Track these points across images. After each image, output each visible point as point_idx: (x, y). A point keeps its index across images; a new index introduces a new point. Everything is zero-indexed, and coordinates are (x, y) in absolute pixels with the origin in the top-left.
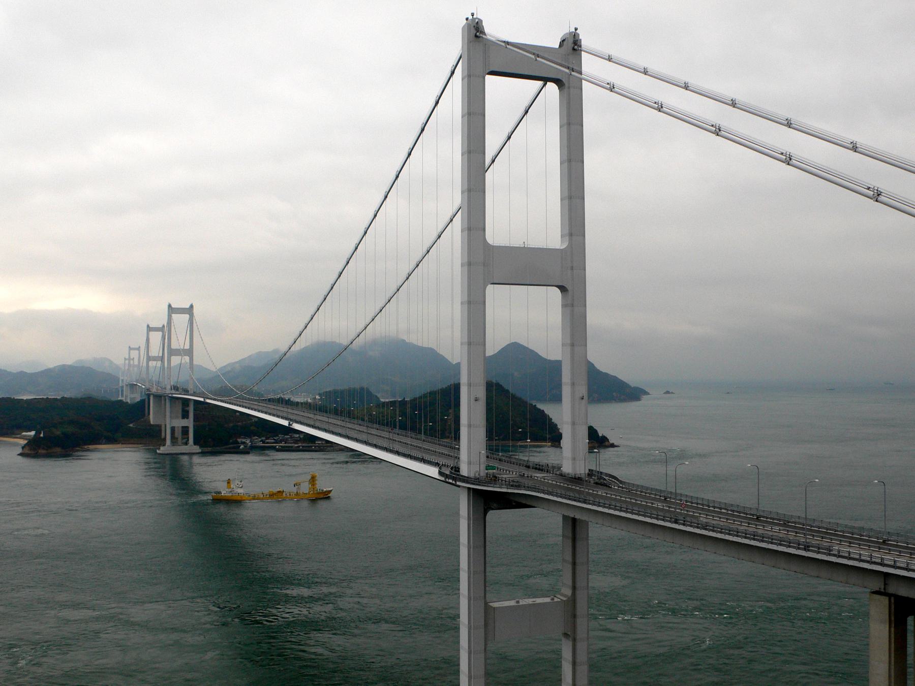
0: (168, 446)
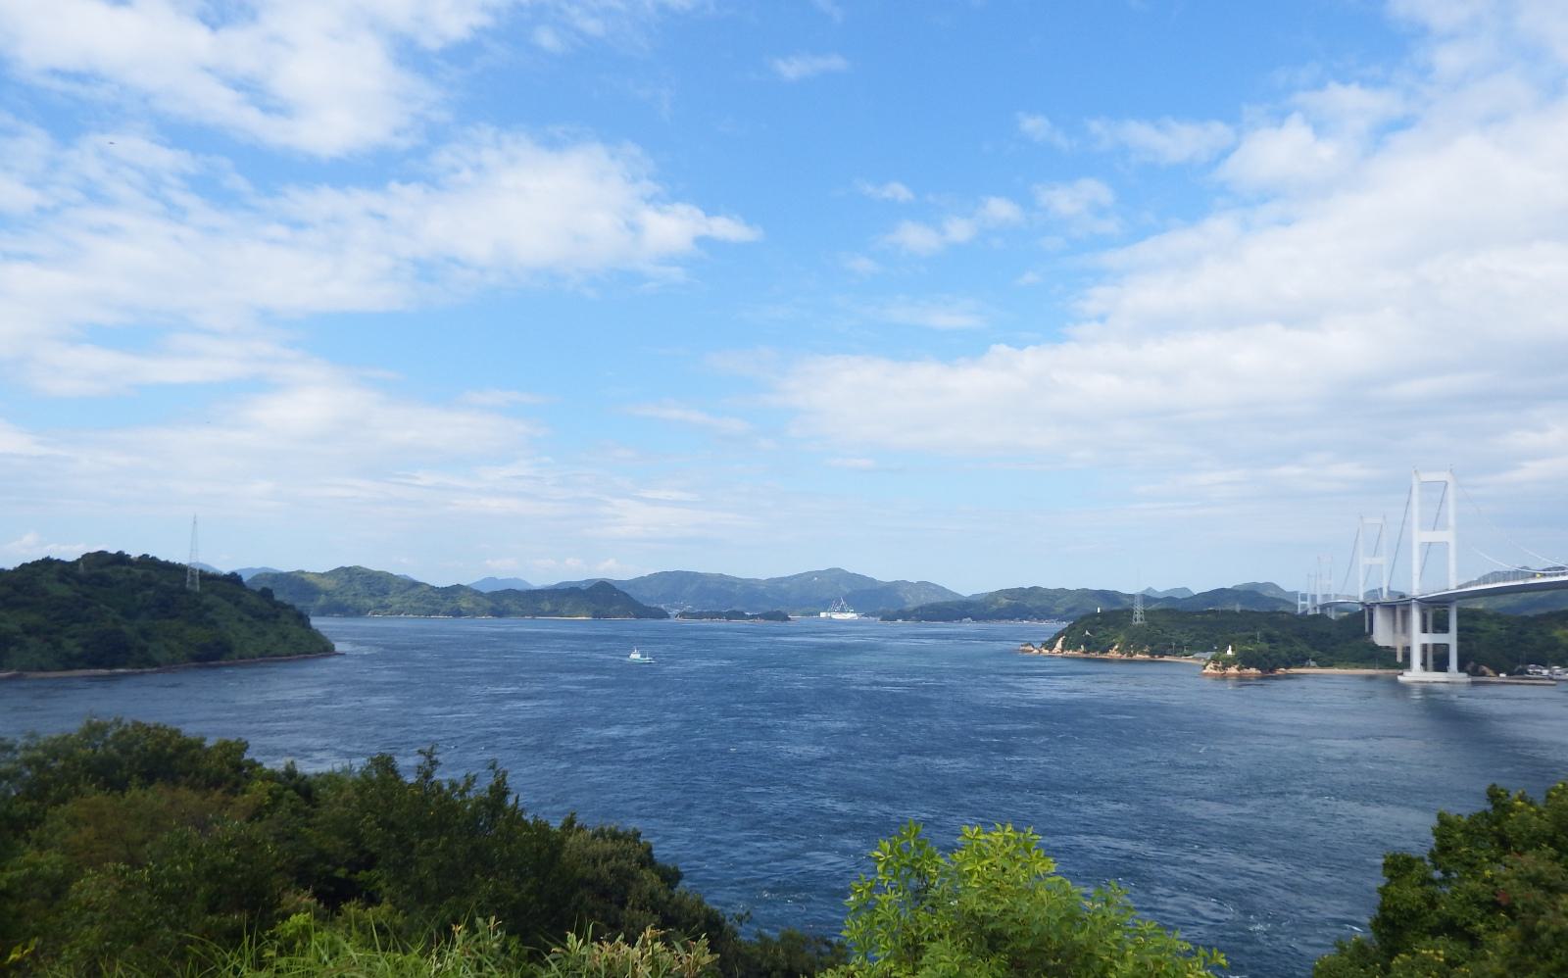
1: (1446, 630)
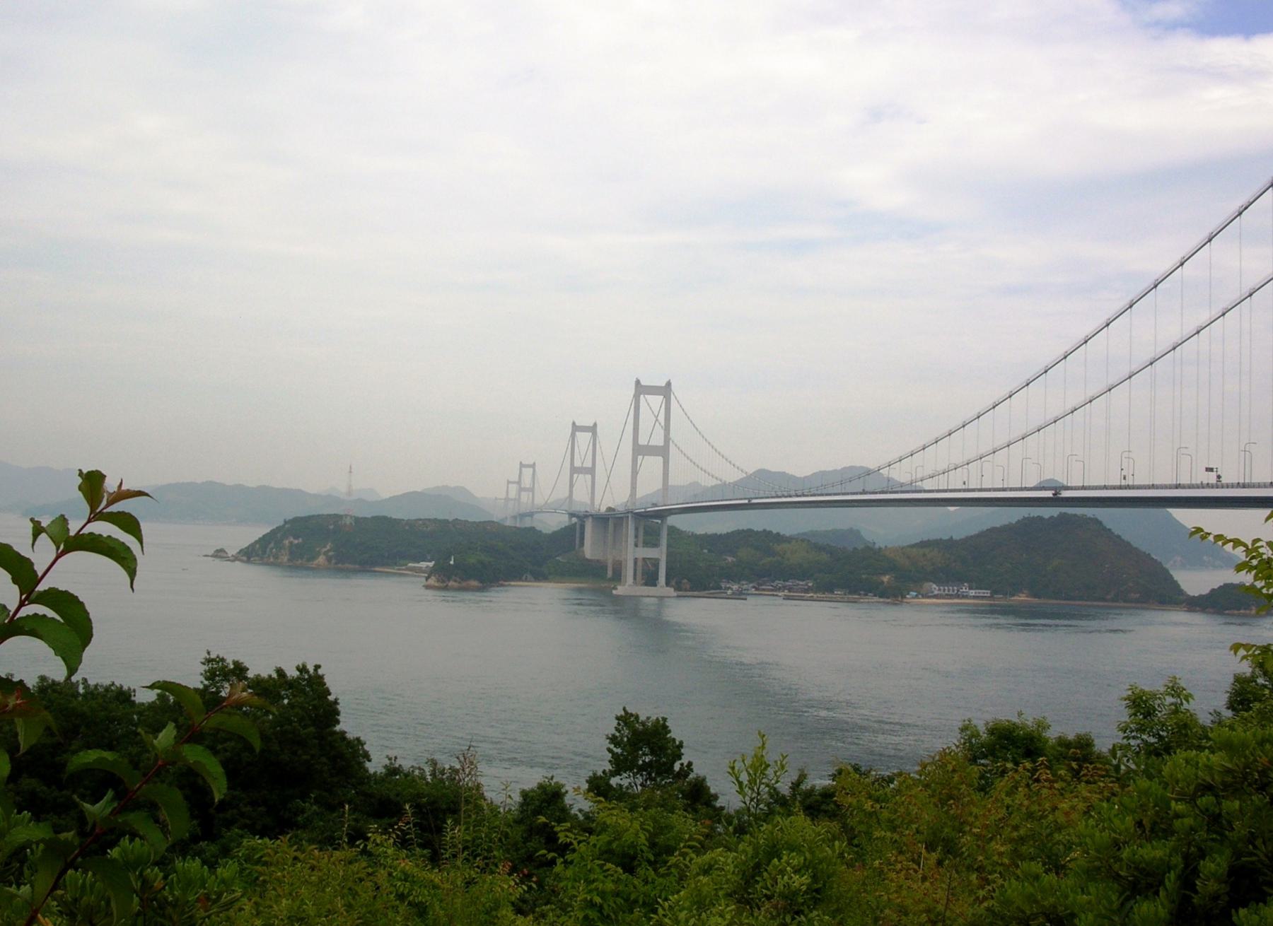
0: (630, 586)
1: (655, 545)
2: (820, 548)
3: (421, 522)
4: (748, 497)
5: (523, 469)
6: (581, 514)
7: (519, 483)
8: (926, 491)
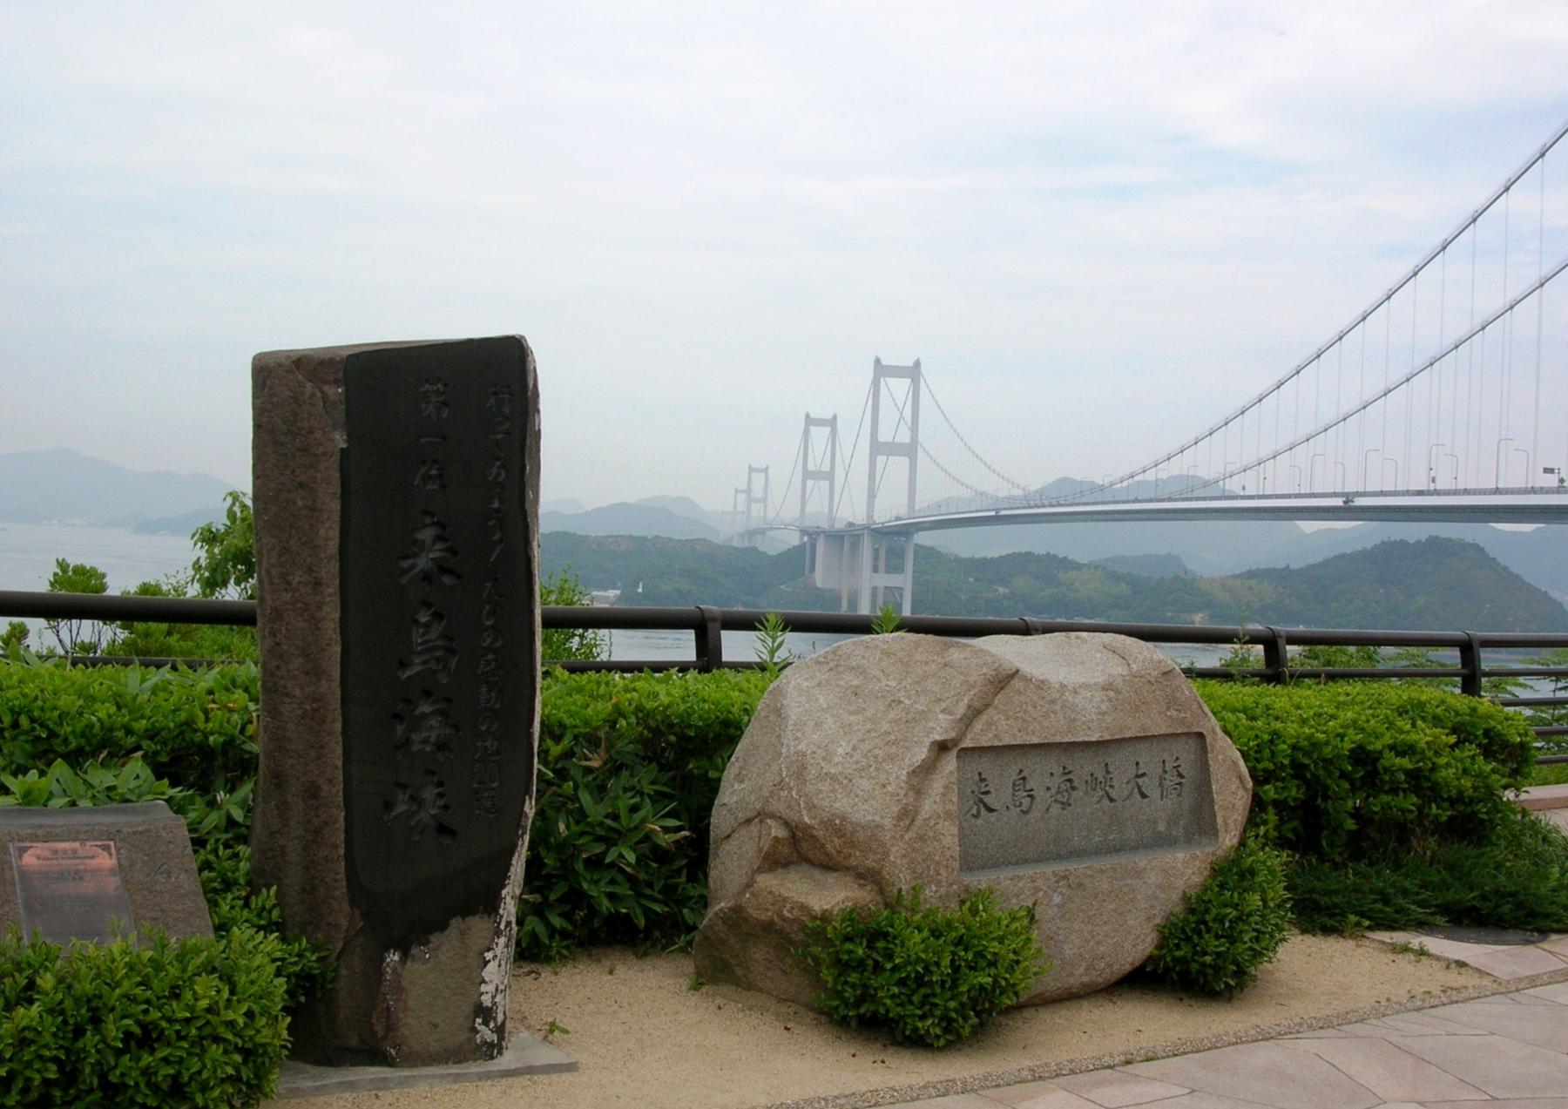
1: (895, 568)
2: (1116, 577)
3: (611, 540)
4: (997, 507)
5: (753, 475)
6: (811, 531)
7: (748, 491)
8: (1236, 497)
